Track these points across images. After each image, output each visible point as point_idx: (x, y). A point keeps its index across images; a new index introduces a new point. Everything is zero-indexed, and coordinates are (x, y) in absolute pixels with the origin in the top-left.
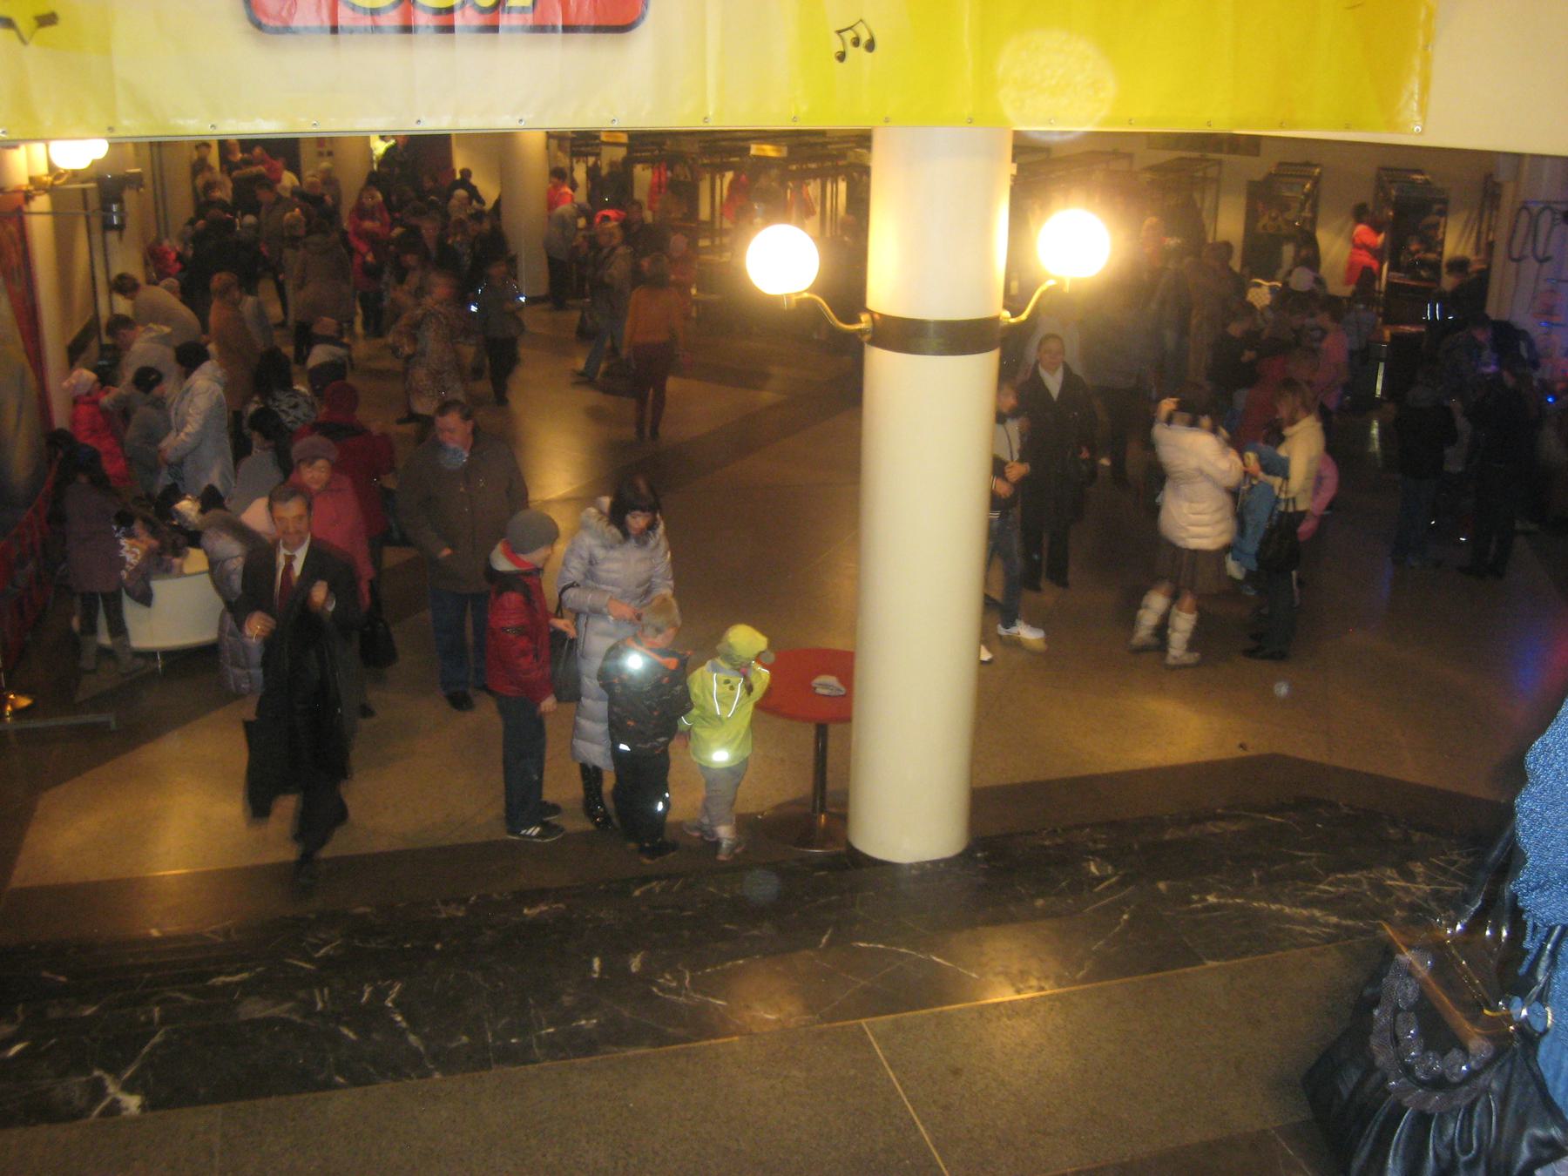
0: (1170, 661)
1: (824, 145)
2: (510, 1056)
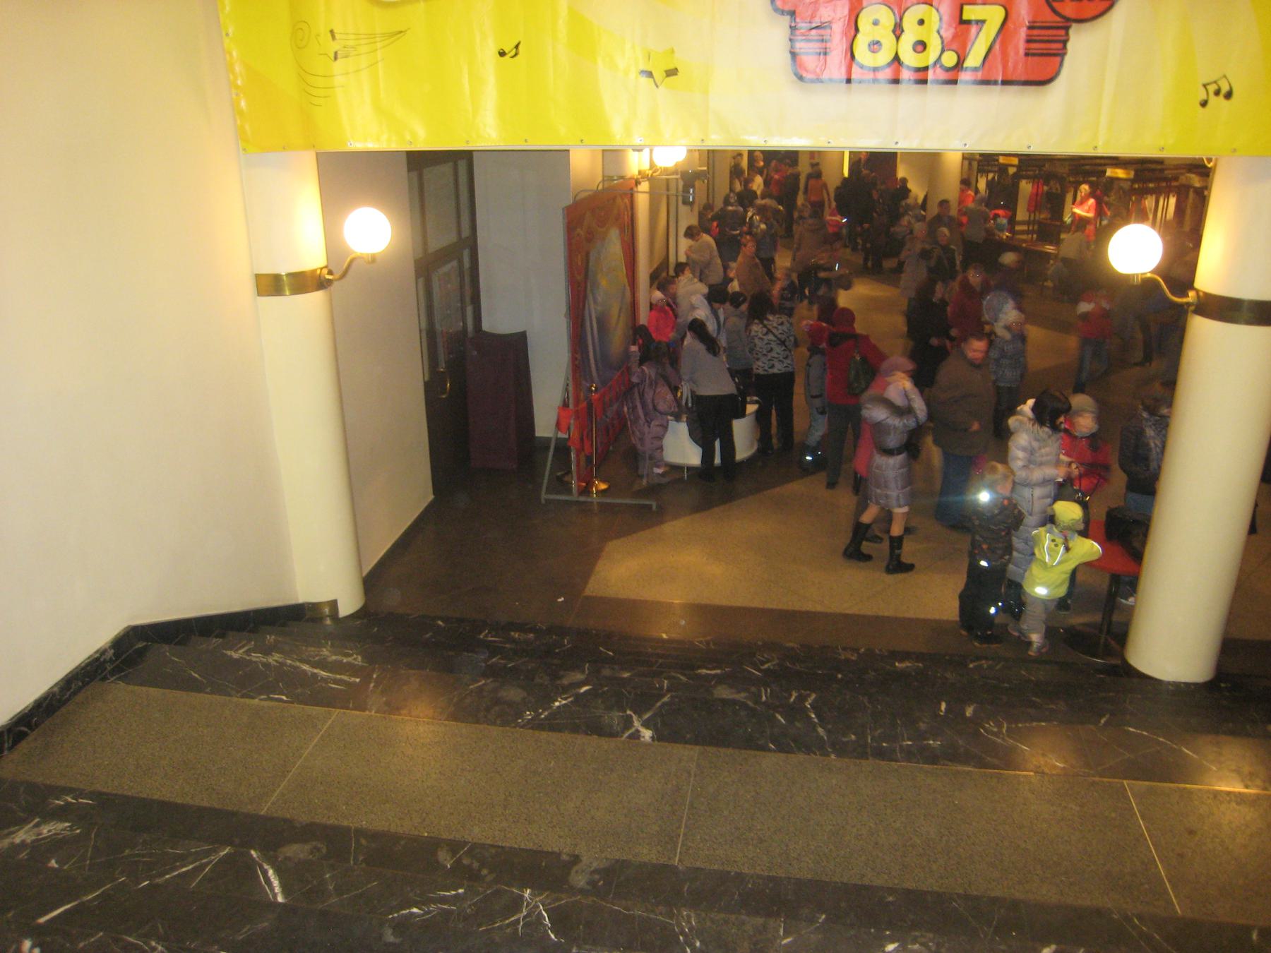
1: (1162, 170)
2: (881, 754)
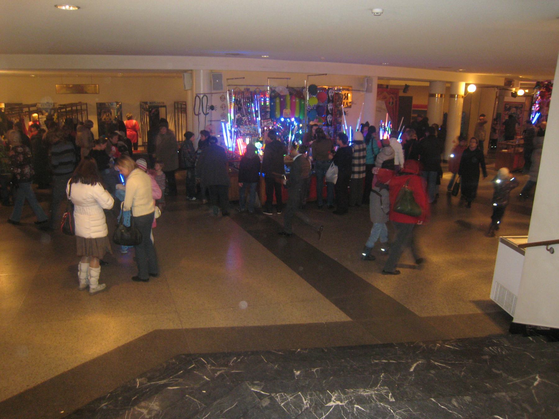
0: (92, 291)
